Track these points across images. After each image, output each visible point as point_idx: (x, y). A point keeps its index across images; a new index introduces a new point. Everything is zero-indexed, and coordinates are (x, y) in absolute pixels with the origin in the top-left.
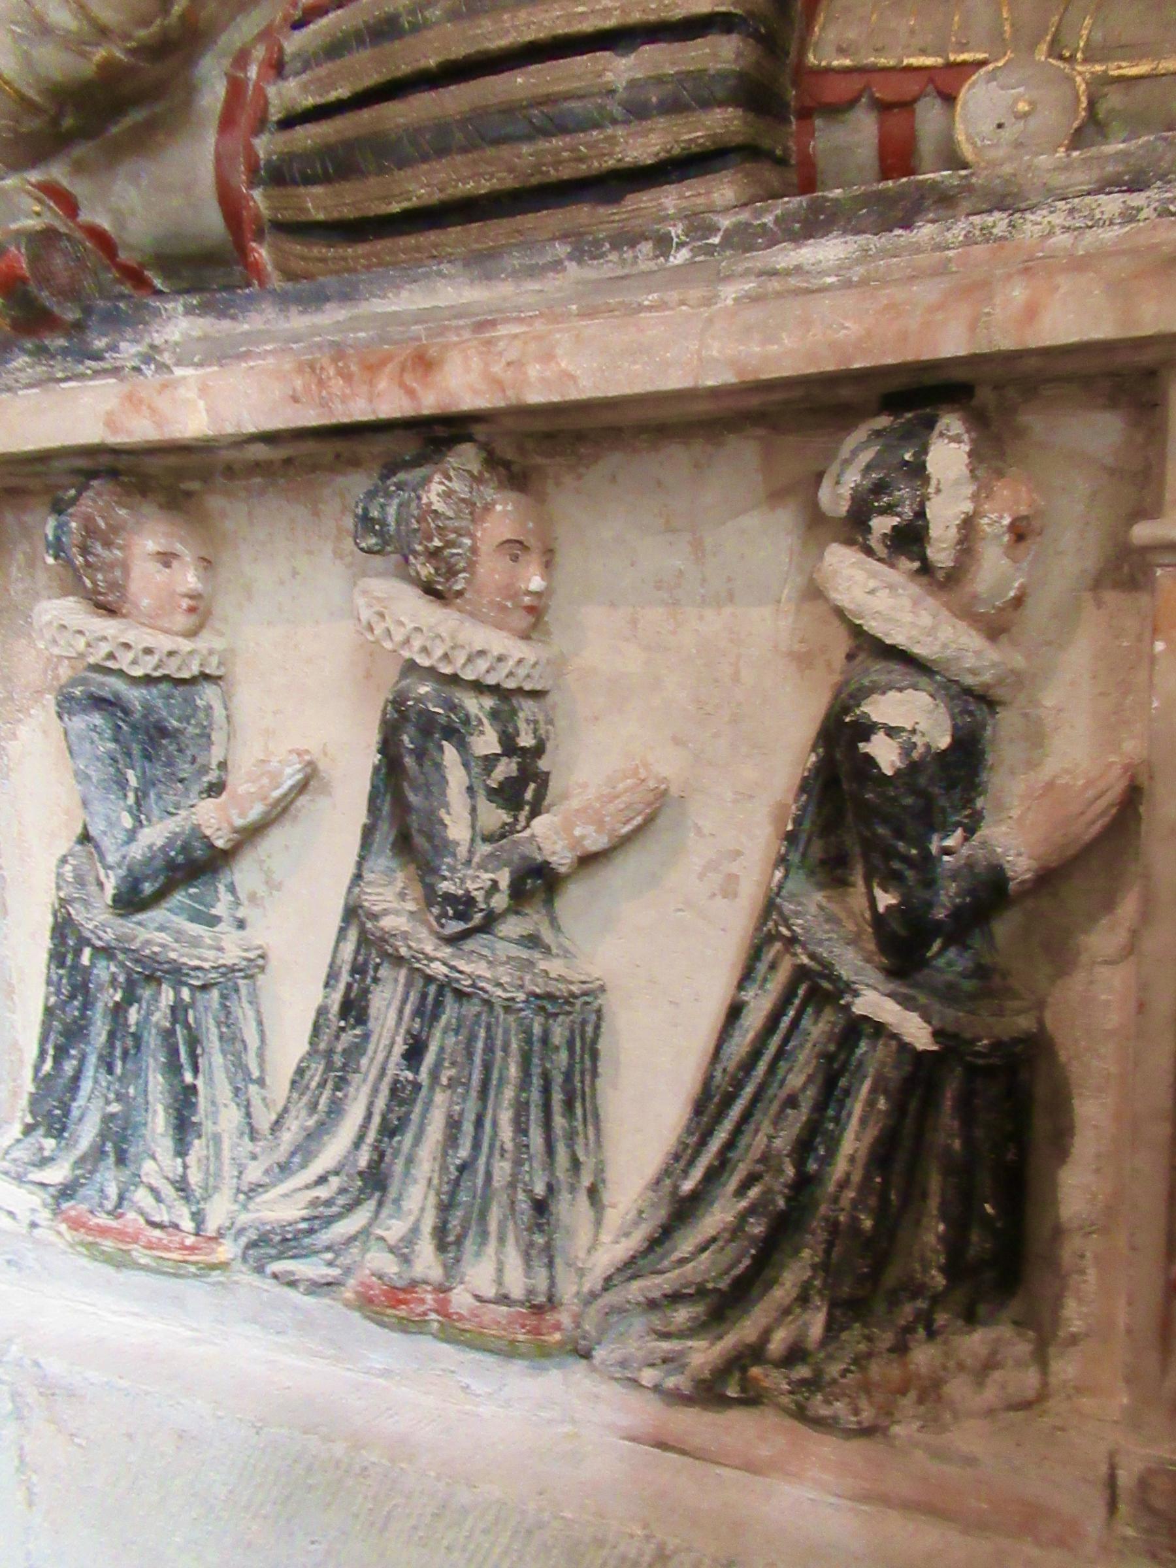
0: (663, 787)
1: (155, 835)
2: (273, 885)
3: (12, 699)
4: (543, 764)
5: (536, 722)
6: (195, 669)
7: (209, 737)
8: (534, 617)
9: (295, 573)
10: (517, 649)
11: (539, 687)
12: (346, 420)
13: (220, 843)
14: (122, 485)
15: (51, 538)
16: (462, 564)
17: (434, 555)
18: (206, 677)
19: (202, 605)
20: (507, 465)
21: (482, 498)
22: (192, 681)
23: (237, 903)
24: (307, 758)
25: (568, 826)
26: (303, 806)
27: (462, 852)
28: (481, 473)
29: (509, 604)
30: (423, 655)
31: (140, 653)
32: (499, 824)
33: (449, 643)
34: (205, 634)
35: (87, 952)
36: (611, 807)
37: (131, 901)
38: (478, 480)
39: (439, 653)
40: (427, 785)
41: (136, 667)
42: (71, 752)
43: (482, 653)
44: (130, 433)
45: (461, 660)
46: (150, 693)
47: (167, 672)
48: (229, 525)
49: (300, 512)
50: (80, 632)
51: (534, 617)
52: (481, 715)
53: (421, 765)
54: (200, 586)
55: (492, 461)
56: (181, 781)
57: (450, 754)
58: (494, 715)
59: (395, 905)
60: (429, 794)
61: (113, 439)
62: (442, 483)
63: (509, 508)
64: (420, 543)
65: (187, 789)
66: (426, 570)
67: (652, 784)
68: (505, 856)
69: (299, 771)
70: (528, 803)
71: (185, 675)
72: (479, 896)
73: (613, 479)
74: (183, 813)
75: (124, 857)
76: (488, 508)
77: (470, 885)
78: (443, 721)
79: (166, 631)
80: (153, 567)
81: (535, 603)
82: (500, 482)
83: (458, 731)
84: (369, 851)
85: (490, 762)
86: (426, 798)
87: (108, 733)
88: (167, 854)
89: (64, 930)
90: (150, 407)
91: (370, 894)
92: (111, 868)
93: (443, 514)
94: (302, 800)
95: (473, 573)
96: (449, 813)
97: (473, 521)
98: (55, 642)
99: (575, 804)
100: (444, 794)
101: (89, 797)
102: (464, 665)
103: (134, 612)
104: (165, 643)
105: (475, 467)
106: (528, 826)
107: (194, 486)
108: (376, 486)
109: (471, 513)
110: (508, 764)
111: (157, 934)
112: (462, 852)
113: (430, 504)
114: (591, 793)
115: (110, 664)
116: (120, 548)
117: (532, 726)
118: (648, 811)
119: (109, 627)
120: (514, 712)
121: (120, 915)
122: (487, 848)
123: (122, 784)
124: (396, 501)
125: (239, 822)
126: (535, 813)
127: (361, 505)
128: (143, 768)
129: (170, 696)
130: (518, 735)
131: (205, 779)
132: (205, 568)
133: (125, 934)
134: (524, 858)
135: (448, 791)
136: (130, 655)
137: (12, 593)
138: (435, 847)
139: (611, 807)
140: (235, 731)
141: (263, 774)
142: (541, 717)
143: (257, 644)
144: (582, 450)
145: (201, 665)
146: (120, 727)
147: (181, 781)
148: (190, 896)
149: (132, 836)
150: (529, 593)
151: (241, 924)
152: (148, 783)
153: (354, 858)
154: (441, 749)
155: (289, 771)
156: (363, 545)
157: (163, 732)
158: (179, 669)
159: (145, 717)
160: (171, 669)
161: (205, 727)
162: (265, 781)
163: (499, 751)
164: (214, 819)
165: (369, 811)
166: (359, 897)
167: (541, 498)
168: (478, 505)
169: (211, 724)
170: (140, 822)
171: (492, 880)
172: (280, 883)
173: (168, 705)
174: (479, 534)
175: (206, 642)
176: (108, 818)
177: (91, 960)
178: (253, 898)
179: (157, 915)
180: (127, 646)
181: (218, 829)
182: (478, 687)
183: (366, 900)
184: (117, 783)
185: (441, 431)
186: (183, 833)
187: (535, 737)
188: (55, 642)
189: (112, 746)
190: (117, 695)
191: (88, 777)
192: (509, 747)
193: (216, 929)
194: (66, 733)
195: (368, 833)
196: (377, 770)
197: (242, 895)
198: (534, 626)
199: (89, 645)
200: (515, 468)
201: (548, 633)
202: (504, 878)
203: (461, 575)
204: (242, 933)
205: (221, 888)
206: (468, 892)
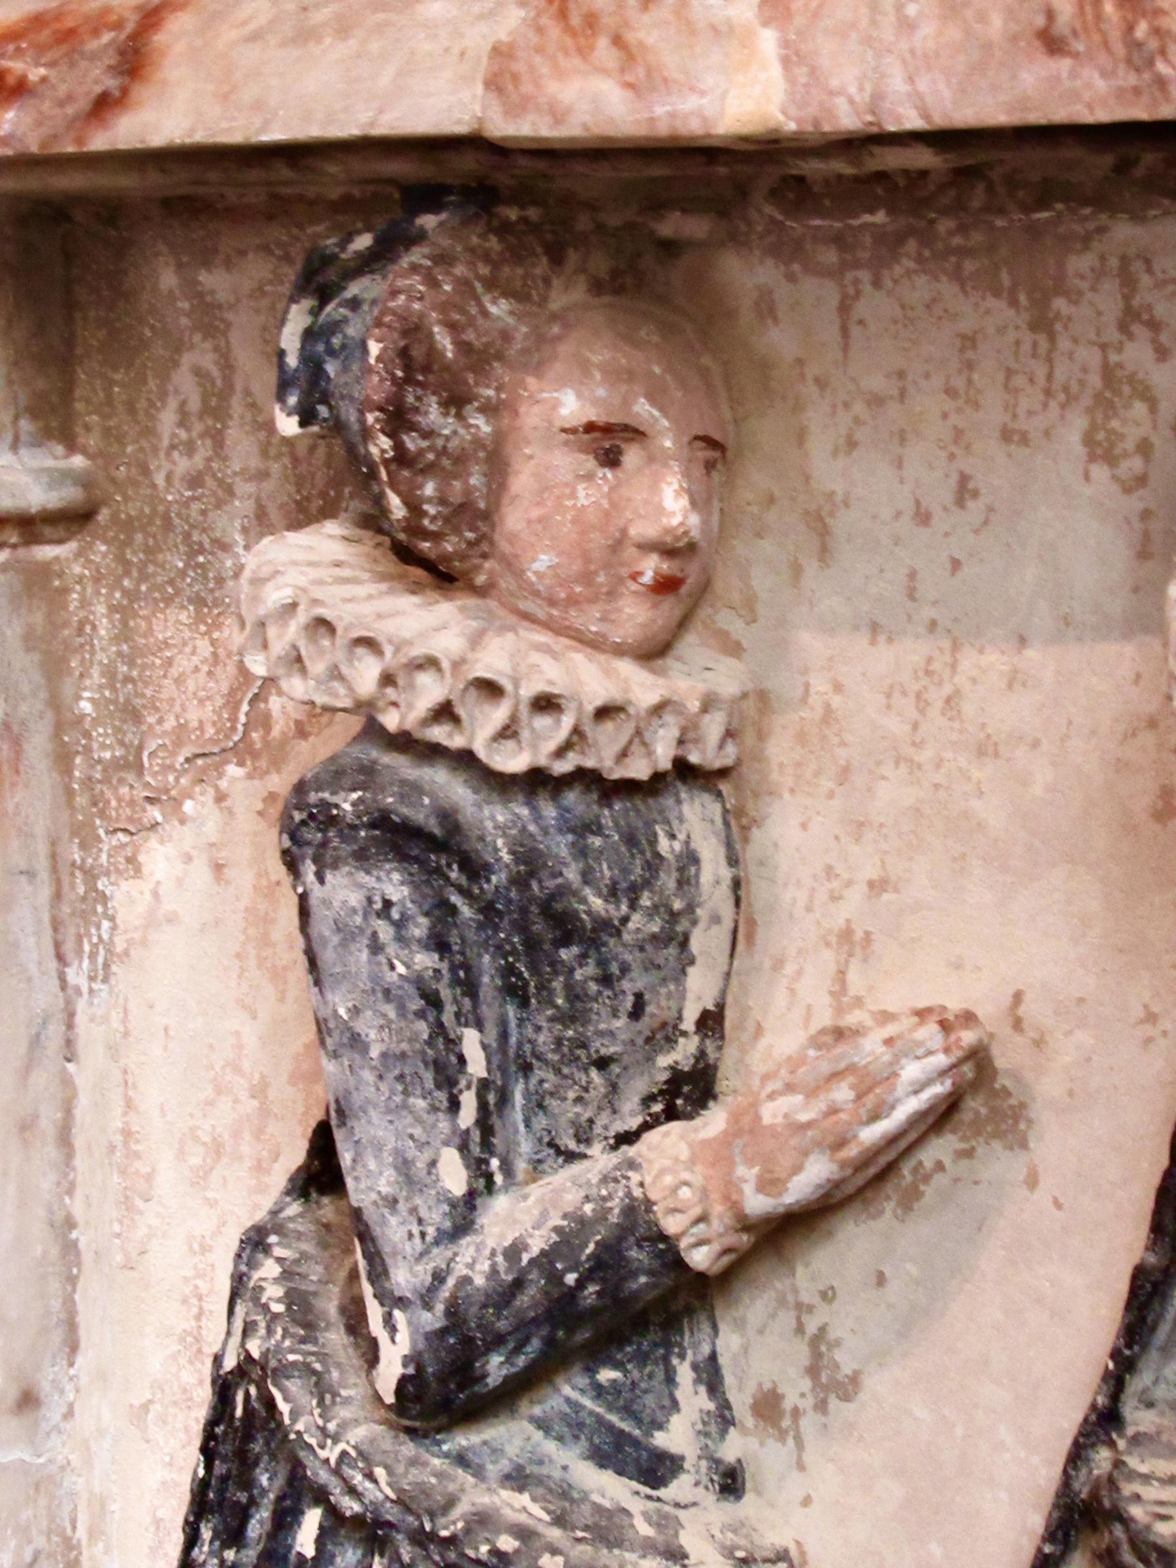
1: (526, 1217)
2: (833, 1385)
3: (140, 769)
6: (663, 755)
7: (684, 943)
9: (964, 491)
13: (700, 1258)
14: (503, 229)
15: (292, 361)
18: (684, 771)
19: (692, 572)
22: (656, 784)
23: (723, 1418)
24: (968, 1037)
26: (940, 1166)
31: (524, 710)
34: (691, 645)
35: (312, 1519)
37: (440, 1398)
41: (510, 744)
42: (313, 964)
44: (558, 115)
46: (537, 817)
47: (590, 763)
48: (780, 341)
49: (998, 318)
50: (369, 643)
54: (694, 520)
56: (602, 1063)
61: (503, 126)
65: (614, 1088)
69: (943, 1073)
71: (639, 770)
74: (601, 1159)
75: (439, 1277)
79: (594, 644)
80: (567, 462)
87: (420, 928)
88: (555, 1278)
89: (241, 1437)
90: (618, 41)
91: (1146, 1478)
92: (401, 1302)
94: (939, 1149)
98: (297, 661)
101: (357, 1100)
103: (506, 583)
104: (590, 679)
107: (695, 227)
111: (506, 1494)
115: (439, 733)
116: (490, 410)
119: (431, 624)
121: (411, 1432)
123: (448, 1073)
125: (757, 1204)
128: (503, 1024)
129: (591, 827)
131: (664, 1061)
132: (709, 466)
133: (425, 1490)
136: (499, 714)
137: (160, 480)
140: (752, 923)
141: (835, 1076)
143: (838, 688)
145: (681, 742)
146: (453, 910)
147: (602, 1063)
148: (599, 1391)
149: (463, 1216)
151: (731, 1482)
152: (513, 1061)
155: (911, 1071)
157: (567, 927)
158: (624, 754)
159: (520, 882)
160: (603, 753)
161: (674, 916)
162: (843, 1093)
164: (682, 1178)
166: (1111, 1481)
169: (690, 908)
170: (489, 1177)
172: (855, 1379)
173: (581, 852)
175: (699, 675)
176: (404, 1166)
177: (320, 1542)
178: (768, 1406)
179: (510, 1436)
180: (490, 689)
181: (702, 1219)
183: (1137, 1498)
184: (438, 1066)
186: (602, 1215)
188: (297, 661)
189: (425, 960)
190: (448, 816)
191: (356, 1042)
193: (662, 1493)
194: (304, 912)
197: (740, 1400)
199: (387, 679)
204: (730, 1510)
205: (684, 1373)
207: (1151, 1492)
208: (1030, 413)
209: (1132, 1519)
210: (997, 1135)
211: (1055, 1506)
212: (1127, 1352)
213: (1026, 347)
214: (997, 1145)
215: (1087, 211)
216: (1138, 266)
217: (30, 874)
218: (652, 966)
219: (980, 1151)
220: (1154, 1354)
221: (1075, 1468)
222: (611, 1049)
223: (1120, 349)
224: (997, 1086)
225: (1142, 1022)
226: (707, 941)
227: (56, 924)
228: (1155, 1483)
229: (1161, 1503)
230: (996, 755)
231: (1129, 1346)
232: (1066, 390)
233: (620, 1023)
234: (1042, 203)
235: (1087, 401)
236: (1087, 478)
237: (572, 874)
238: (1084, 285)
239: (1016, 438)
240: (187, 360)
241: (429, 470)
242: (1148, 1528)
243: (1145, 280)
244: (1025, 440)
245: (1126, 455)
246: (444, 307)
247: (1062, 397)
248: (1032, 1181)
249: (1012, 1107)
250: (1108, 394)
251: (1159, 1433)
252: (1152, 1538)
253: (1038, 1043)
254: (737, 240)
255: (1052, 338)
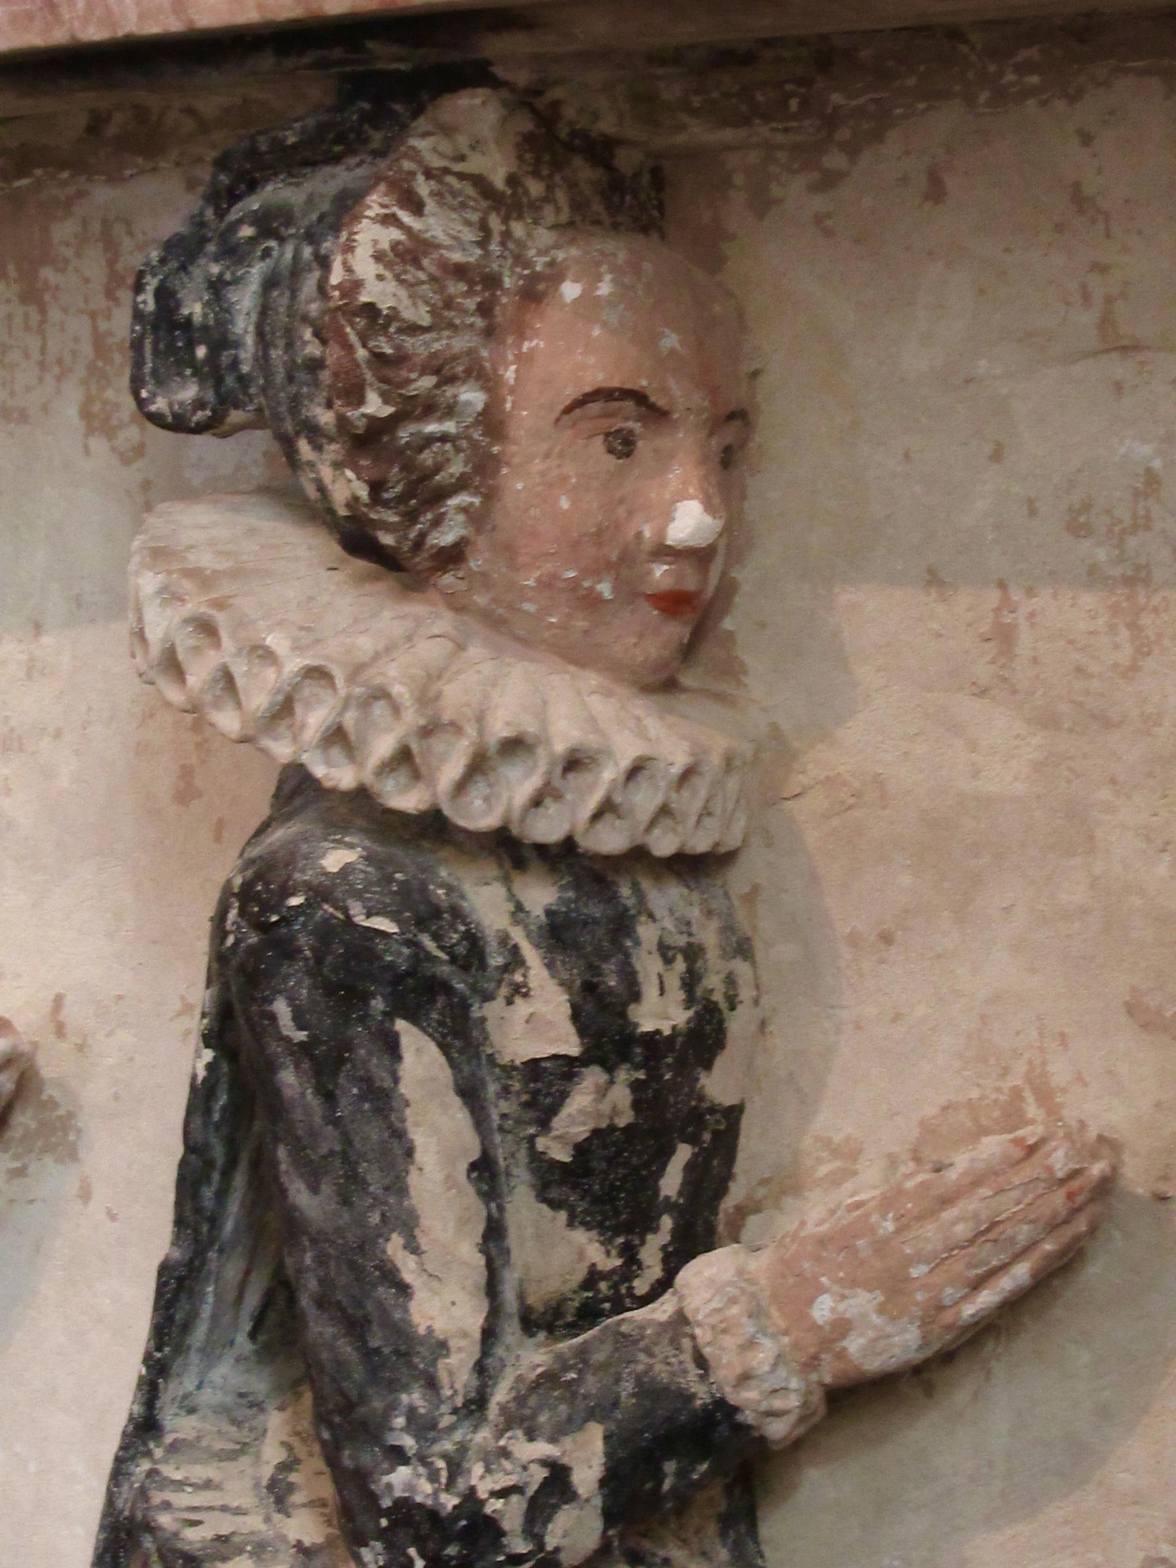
0: (1097, 1169)
4: (718, 1085)
5: (693, 953)
8: (689, 627)
10: (627, 730)
11: (701, 844)
12: (94, 33)
16: (457, 468)
17: (367, 441)
20: (600, 150)
21: (520, 260)
25: (795, 1292)
27: (457, 1370)
28: (512, 180)
29: (605, 589)
30: (336, 752)
32: (580, 1274)
33: (412, 718)
36: (930, 1235)
38: (507, 203)
39: (383, 746)
40: (348, 1157)
43: (515, 746)
45: (451, 770)
51: (689, 627)
52: (518, 936)
53: (329, 1098)
55: (549, 143)
57: (420, 1060)
58: (557, 933)
59: (254, 1523)
60: (351, 1187)
62: (389, 220)
63: (605, 289)
64: (329, 405)
66: (346, 487)
67: (1059, 1160)
68: (591, 1385)
70: (669, 1206)
72: (510, 1514)
73: (936, 192)
76: (535, 293)
77: (481, 1480)
78: (398, 957)
81: (690, 583)
82: (578, 206)
83: (447, 989)
84: (180, 1349)
85: (545, 1083)
86: (345, 1201)
91: (179, 1485)
93: (394, 315)
95: (490, 496)
96: (413, 1247)
97: (489, 333)
99: (814, 1213)
100: (399, 1188)
102: (461, 786)
105: (496, 166)
106: (664, 1285)
108: (199, 223)
109: (484, 310)
110: (602, 1092)
112: (457, 1370)
113: (353, 286)
114: (868, 1183)
117: (680, 965)
118: (1048, 1247)
120: (622, 926)
122: (531, 1357)
124: (256, 272)
126: (693, 1240)
127: (152, 283)
130: (635, 996)
134: (648, 1390)
135: (413, 1179)
138: (369, 1354)
139: (930, 1235)
142: (709, 936)
144: (836, 98)
150: (663, 552)
153: (133, 1368)
154: (392, 1047)
156: (160, 405)
163: (572, 1047)
165: (180, 1222)
167: (709, 250)
168: (507, 282)
171: (546, 1463)
174: (510, 374)
182: (507, 849)
183: (167, 1506)
185: (389, 58)
187: (690, 1001)
192: (606, 1031)
195: (176, 1289)
196: (201, 1097)
198: (688, 651)
200: (627, 160)
201: (732, 670)
202: (588, 1467)
203: (453, 502)
206: (470, 1495)
207: (182, 1499)
208: (28, 389)
209: (160, 1528)
210: (47, 1149)
211: (102, 1527)
212: (158, 1355)
213: (18, 321)
214: (48, 1160)
215: (65, 175)
216: (118, 229)
219: (32, 1169)
220: (194, 1357)
221: (117, 1485)
223: (108, 317)
224: (44, 1097)
225: (180, 1014)
228: (189, 1489)
229: (194, 1509)
230: (21, 749)
231: (159, 1348)
232: (60, 362)
234: (22, 169)
235: (81, 372)
236: (87, 450)
238: (69, 252)
239: (16, 415)
242: (176, 1535)
243: (127, 244)
244: (24, 417)
245: (121, 426)
247: (57, 370)
248: (85, 1195)
249: (60, 1118)
250: (100, 364)
251: (199, 1438)
252: (180, 1545)
253: (81, 1048)
255: (43, 312)
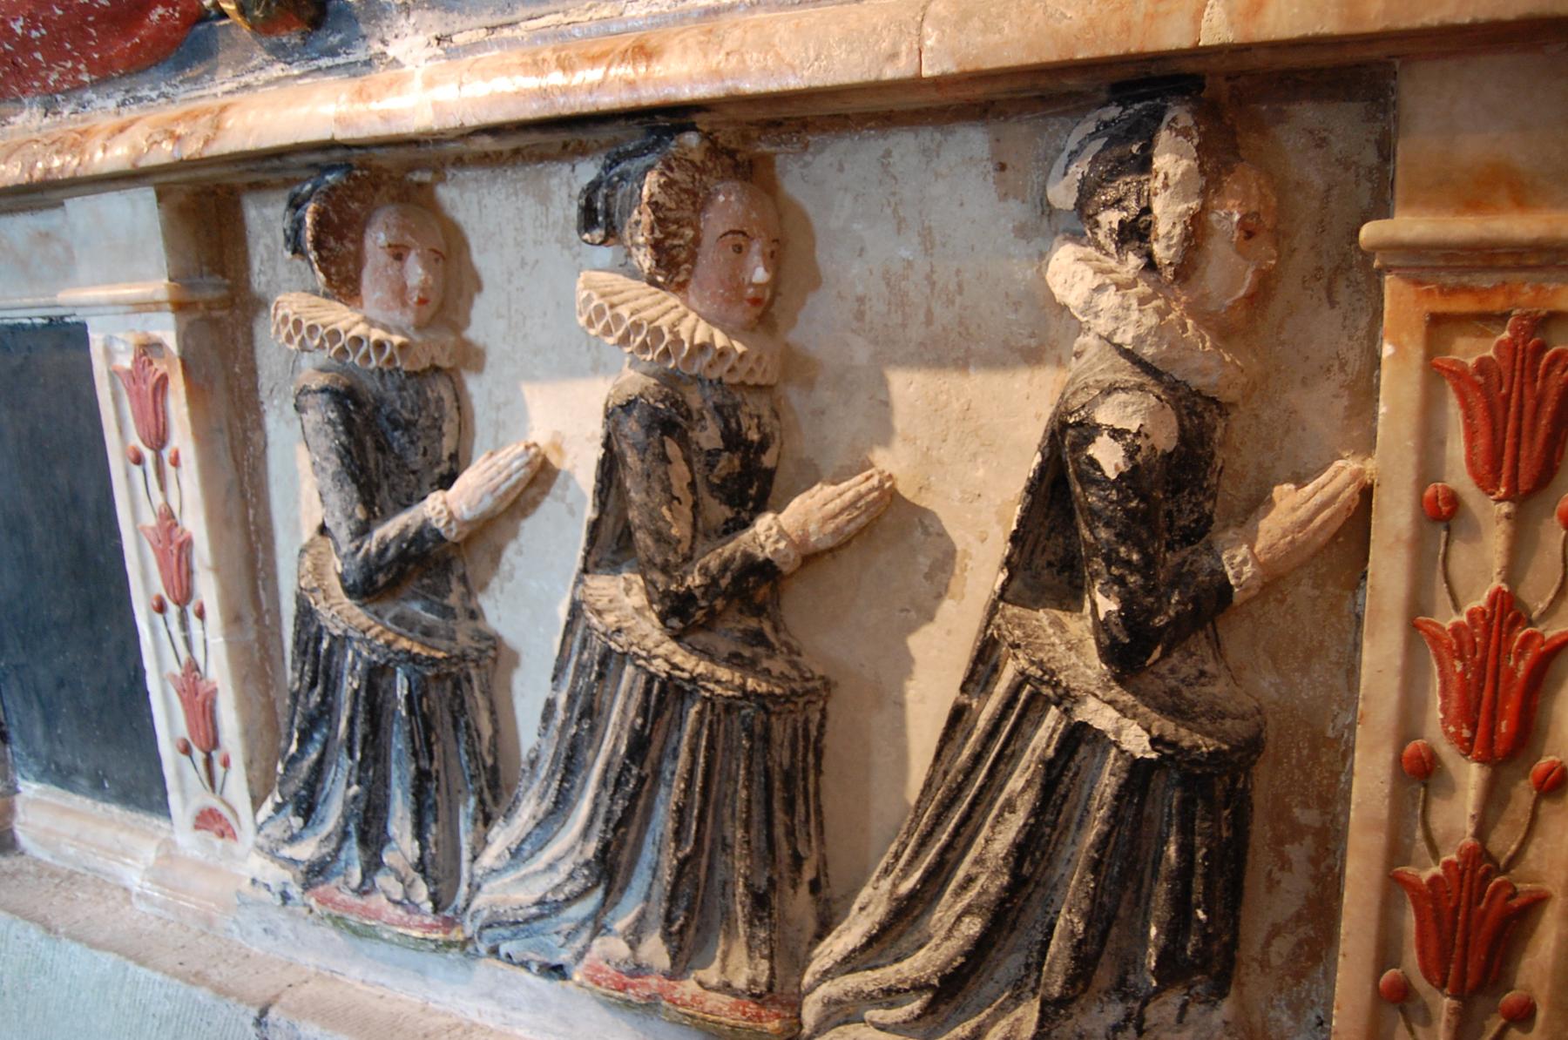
7: (440, 429)
18: (436, 369)
56: (414, 472)
65: (419, 481)
131: (437, 471)
169: (441, 417)
217: (221, 431)
218: (428, 437)
222: (415, 467)
226: (448, 427)
227: (232, 447)
233: (419, 458)
237: (398, 405)
240: (262, 241)
241: (334, 263)
246: (334, 206)
254: (443, 180)
